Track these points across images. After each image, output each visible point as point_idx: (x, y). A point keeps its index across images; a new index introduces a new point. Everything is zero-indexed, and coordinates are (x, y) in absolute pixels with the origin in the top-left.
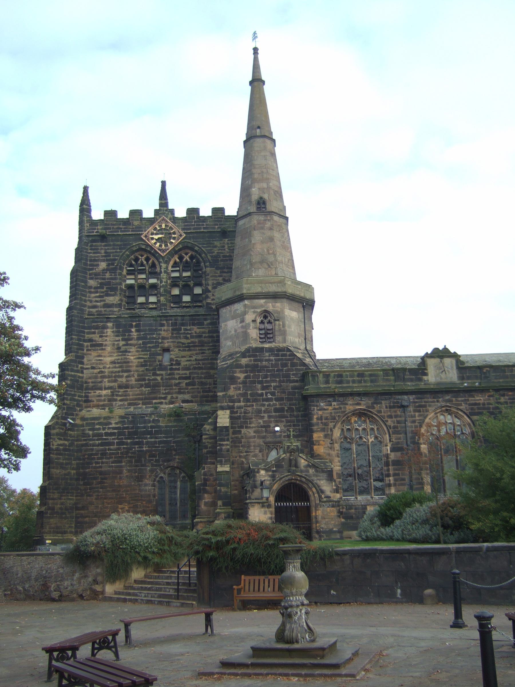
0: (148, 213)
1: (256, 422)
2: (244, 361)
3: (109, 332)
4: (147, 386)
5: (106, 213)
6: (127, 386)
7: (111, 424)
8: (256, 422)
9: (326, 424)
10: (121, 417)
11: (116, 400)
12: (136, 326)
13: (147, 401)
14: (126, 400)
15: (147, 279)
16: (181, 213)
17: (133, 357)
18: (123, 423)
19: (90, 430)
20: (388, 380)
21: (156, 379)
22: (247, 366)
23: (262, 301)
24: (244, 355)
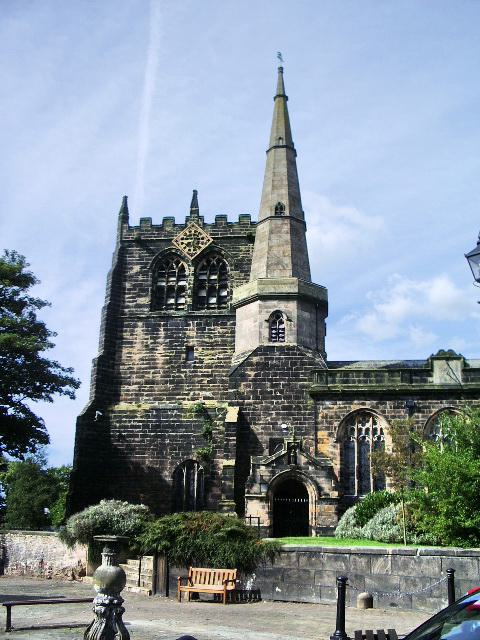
0: (180, 220)
2: (255, 359)
4: (171, 382)
5: (142, 220)
6: (153, 382)
7: (136, 417)
9: (331, 423)
10: (146, 411)
11: (142, 395)
13: (171, 396)
14: (152, 395)
15: (178, 281)
16: (210, 220)
19: (117, 422)
21: (180, 376)
22: (258, 364)
23: (275, 302)
24: (255, 353)
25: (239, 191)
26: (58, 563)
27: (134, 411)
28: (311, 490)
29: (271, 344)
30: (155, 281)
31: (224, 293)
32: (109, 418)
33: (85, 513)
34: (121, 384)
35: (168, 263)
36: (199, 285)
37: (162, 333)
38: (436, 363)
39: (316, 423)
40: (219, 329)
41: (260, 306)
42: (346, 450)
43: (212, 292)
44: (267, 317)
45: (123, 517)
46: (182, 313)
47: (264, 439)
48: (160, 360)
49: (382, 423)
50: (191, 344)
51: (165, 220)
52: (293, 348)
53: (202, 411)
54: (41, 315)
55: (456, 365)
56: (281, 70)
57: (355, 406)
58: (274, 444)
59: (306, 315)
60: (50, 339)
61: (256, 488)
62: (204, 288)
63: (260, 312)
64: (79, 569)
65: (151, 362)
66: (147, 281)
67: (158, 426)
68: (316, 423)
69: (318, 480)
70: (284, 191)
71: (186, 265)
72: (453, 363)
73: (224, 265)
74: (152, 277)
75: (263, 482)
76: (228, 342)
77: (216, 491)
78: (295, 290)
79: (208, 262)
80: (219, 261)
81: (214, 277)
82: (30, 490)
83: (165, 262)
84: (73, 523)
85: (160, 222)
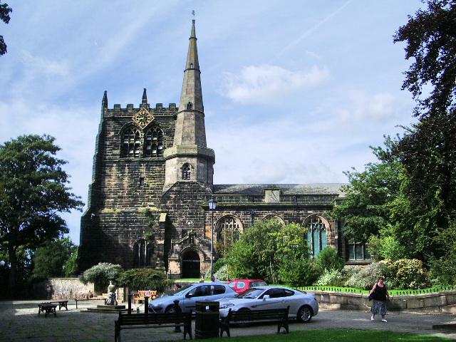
0: (136, 106)
1: (179, 220)
2: (175, 189)
3: (114, 169)
4: (132, 197)
5: (115, 106)
6: (122, 197)
8: (179, 220)
10: (118, 213)
12: (128, 166)
13: (132, 205)
15: (135, 141)
16: (153, 106)
17: (126, 181)
18: (119, 216)
20: (244, 201)
23: (186, 159)
24: (175, 185)
25: (169, 90)
26: (79, 292)
27: (112, 213)
28: (201, 256)
29: (184, 181)
30: (123, 141)
31: (161, 148)
32: (99, 217)
33: (92, 269)
34: (105, 198)
35: (130, 130)
36: (147, 143)
37: (127, 170)
38: (267, 192)
39: (205, 222)
40: (157, 168)
41: (178, 160)
42: (219, 237)
43: (154, 147)
44: (181, 166)
45: (109, 270)
46: (137, 159)
47: (179, 230)
48: (126, 185)
49: (238, 222)
50: (142, 176)
51: (128, 106)
52: (194, 183)
53: (149, 213)
54: (64, 168)
55: (277, 193)
56: (194, 21)
57: (224, 214)
58: (184, 232)
59: (202, 165)
60: (68, 179)
61: (173, 255)
62: (150, 145)
63: (177, 164)
64: (90, 294)
65: (121, 186)
66: (118, 141)
67: (124, 222)
68: (205, 222)
69: (205, 251)
70: (193, 95)
71: (140, 132)
72: (275, 192)
73: (161, 132)
74: (122, 138)
75: (177, 252)
76: (162, 176)
77: (154, 256)
78: (195, 152)
79: (152, 130)
80: (158, 130)
81: (155, 139)
82: (48, 254)
83: (128, 130)
84: (87, 274)
85: (125, 107)
